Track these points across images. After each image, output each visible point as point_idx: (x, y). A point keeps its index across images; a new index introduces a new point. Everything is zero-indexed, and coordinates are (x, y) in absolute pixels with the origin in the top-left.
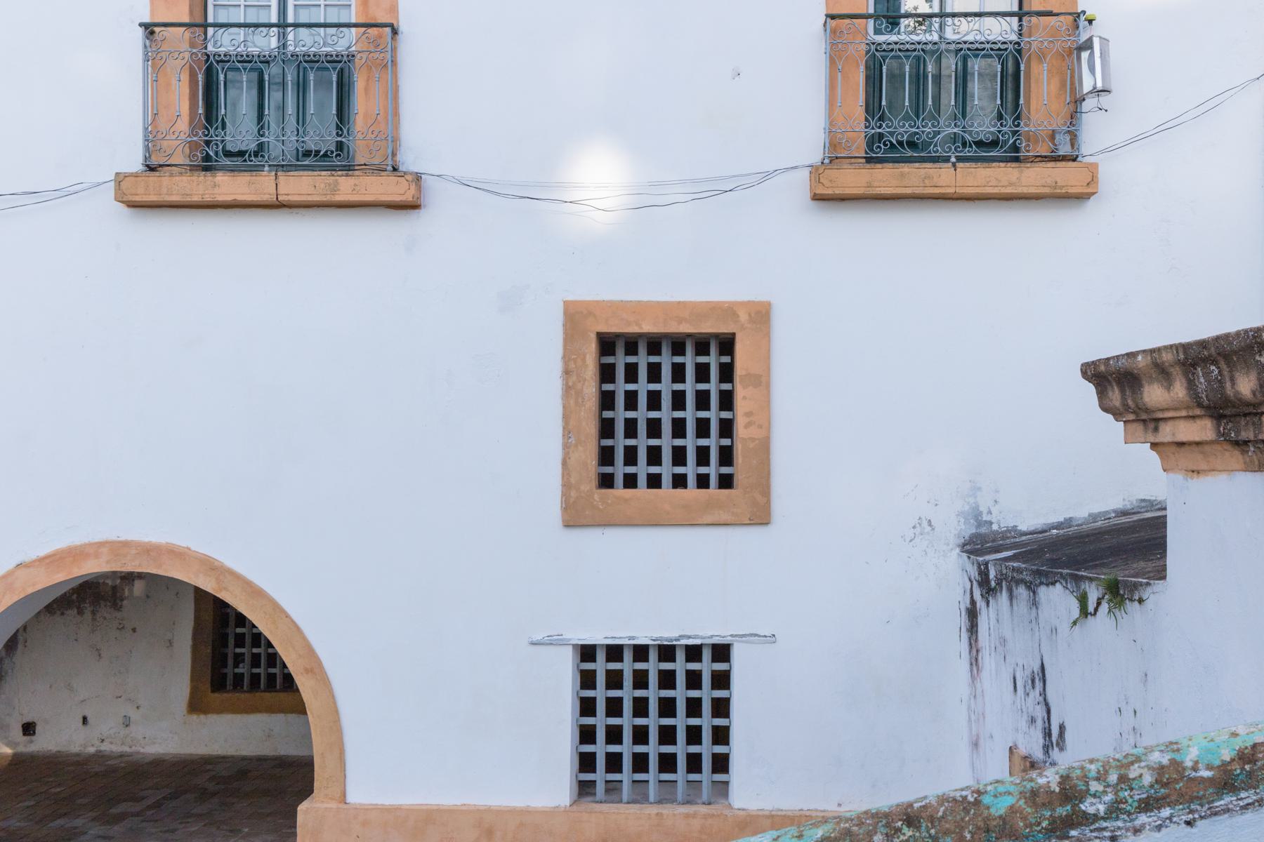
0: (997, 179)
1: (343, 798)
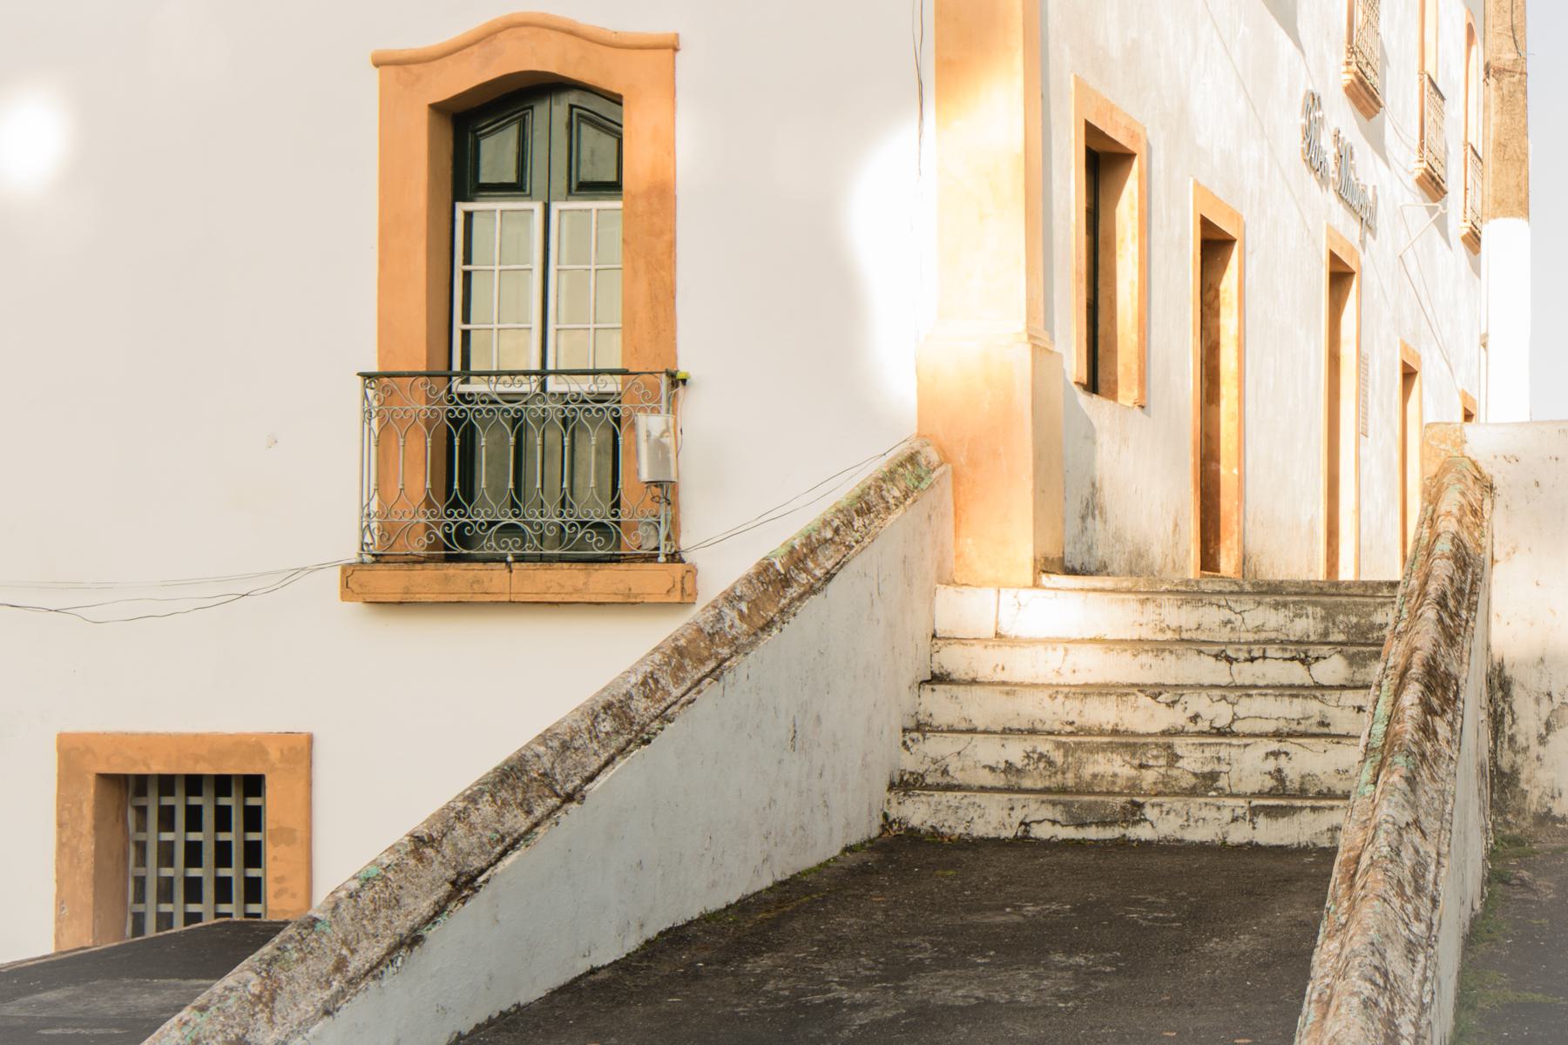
0: (559, 584)
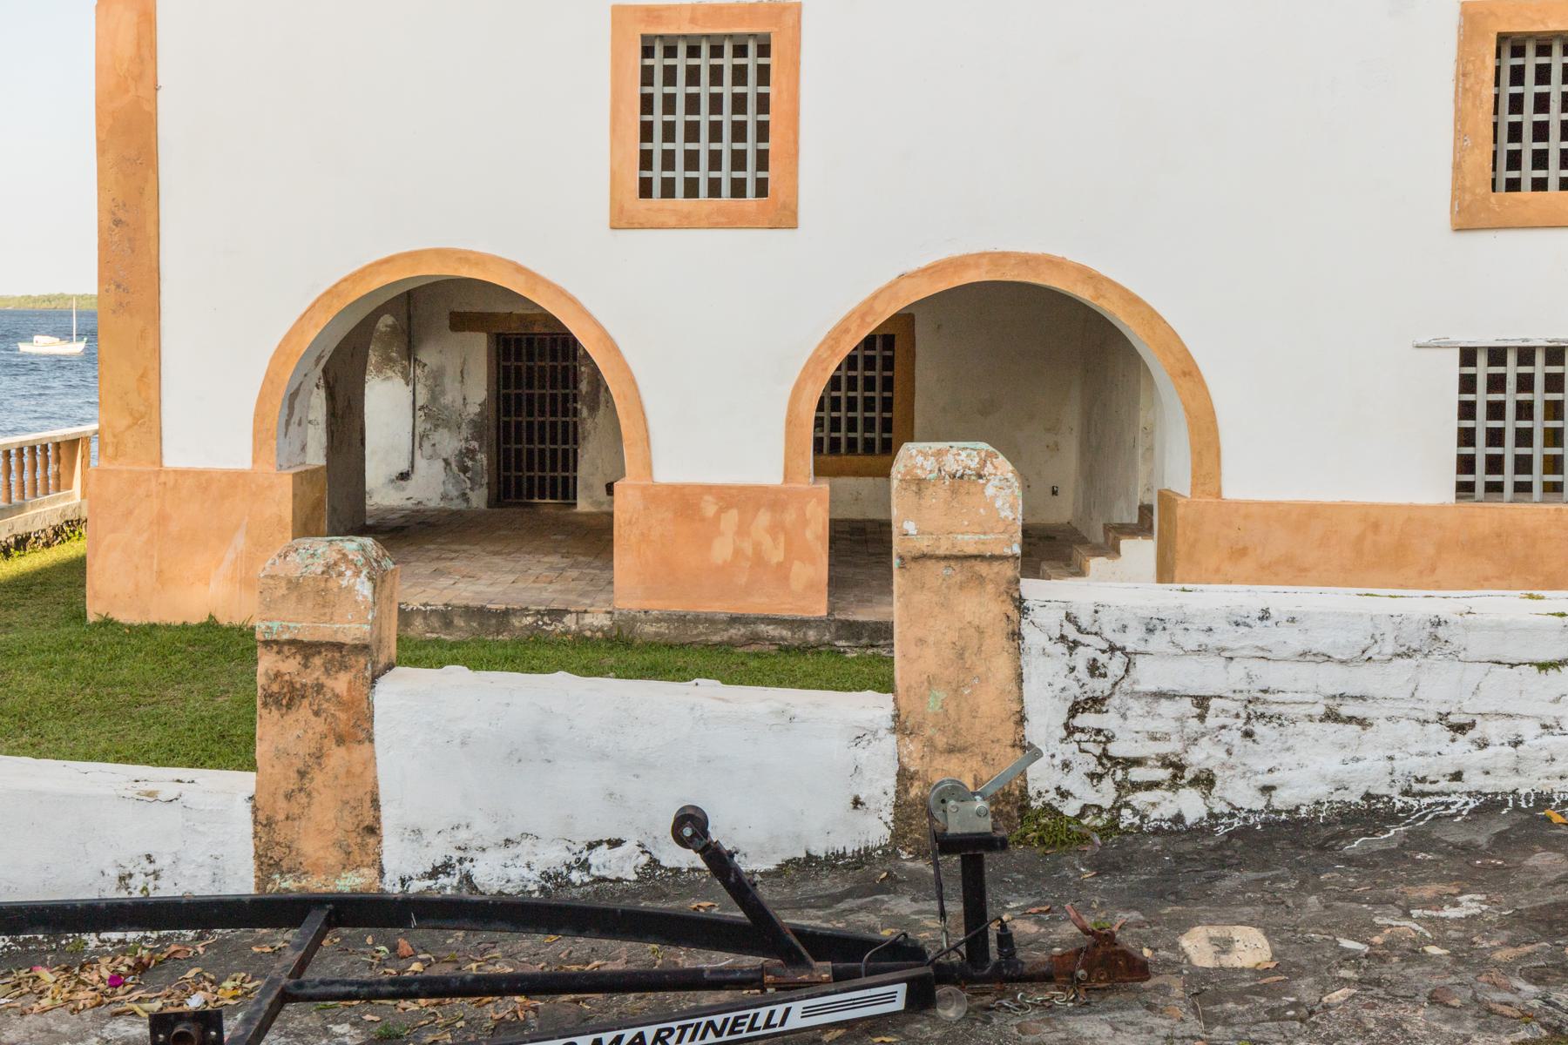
1: (1219, 495)
